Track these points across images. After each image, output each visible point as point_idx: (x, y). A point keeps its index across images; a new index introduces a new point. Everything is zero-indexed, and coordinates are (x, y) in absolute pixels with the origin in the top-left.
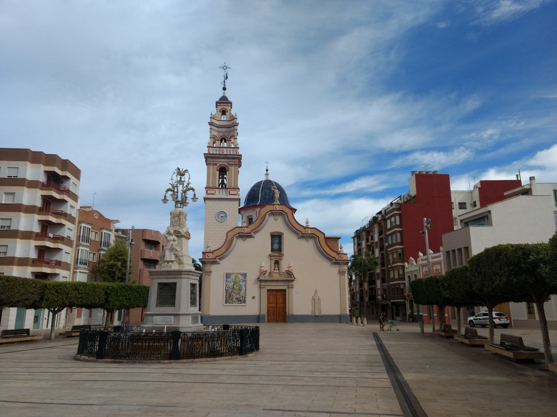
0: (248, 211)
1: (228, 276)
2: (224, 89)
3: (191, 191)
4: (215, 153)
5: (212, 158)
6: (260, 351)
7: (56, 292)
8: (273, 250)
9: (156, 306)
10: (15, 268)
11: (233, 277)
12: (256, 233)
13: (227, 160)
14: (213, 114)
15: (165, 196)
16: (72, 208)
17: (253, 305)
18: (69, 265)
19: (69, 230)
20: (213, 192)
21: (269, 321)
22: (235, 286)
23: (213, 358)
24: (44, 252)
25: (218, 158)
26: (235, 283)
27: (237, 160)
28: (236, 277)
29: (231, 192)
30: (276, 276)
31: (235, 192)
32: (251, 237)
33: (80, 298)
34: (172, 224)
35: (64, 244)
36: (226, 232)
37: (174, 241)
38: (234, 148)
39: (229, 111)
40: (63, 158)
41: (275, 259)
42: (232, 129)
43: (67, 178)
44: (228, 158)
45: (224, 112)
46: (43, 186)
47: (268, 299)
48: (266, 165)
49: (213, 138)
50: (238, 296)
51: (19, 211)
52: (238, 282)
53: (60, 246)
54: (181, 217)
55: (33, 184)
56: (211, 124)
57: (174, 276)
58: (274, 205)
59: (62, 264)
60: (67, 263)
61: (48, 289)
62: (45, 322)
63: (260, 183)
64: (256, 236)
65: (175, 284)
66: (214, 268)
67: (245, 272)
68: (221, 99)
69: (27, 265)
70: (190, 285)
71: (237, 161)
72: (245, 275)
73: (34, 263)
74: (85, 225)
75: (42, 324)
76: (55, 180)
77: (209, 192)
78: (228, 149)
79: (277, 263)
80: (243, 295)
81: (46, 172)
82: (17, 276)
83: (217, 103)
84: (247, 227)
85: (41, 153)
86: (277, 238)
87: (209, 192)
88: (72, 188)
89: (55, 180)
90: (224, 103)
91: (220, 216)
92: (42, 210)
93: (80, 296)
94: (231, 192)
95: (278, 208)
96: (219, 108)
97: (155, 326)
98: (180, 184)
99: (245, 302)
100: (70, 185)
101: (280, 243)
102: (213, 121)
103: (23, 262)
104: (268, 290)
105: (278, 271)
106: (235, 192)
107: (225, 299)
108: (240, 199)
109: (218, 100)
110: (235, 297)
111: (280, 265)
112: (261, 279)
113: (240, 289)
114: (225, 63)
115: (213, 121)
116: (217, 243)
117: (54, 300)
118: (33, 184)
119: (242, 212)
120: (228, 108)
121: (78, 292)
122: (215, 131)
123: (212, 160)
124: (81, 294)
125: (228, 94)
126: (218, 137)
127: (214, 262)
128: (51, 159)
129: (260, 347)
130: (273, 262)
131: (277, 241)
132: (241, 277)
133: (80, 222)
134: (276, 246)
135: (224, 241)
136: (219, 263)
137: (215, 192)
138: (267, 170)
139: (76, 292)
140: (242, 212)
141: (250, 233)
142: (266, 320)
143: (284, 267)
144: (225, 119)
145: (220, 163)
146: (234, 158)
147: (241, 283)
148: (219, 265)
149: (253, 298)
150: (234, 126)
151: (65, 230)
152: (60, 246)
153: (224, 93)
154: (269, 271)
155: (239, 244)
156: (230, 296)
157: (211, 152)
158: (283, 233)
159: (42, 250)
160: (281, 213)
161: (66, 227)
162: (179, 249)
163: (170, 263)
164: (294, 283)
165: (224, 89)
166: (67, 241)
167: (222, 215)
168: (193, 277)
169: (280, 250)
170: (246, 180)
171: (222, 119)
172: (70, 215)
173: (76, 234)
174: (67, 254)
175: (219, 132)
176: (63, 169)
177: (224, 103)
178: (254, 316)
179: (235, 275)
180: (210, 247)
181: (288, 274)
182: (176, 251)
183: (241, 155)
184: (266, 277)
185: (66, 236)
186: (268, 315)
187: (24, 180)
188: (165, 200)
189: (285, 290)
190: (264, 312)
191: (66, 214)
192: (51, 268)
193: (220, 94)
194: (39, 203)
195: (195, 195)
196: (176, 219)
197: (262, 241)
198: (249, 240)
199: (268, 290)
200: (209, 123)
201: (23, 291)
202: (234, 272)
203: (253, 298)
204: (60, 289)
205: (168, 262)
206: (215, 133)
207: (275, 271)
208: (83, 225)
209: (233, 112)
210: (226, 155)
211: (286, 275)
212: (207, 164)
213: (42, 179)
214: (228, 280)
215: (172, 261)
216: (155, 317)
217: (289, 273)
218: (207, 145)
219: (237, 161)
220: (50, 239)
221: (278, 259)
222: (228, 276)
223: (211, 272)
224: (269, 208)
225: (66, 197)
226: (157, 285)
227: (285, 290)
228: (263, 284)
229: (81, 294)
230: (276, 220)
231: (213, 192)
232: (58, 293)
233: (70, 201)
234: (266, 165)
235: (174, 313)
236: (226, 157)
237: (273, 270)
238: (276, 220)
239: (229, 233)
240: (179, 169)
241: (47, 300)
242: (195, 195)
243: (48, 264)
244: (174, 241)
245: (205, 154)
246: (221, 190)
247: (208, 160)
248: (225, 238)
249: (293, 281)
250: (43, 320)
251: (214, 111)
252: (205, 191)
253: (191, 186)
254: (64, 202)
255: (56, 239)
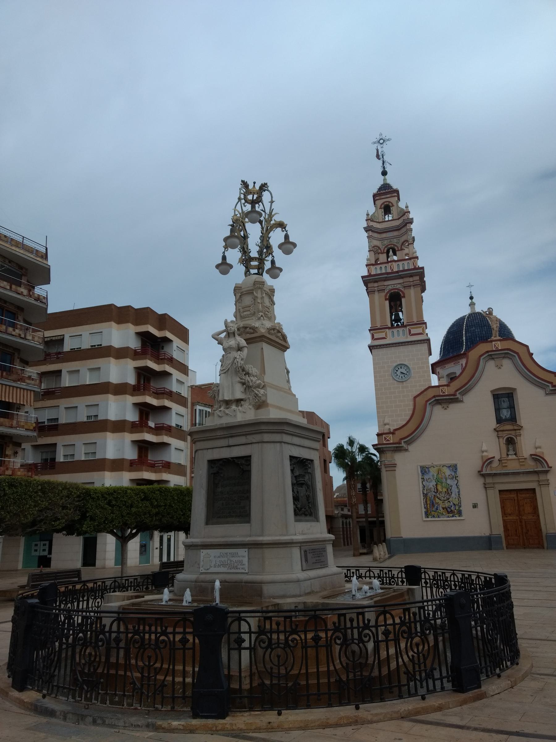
0: (447, 366)
1: (424, 470)
2: (384, 173)
3: (279, 229)
4: (379, 272)
5: (376, 281)
6: (524, 664)
7: (109, 503)
8: (499, 420)
9: (207, 523)
10: (107, 474)
11: (433, 471)
12: (464, 393)
13: (400, 281)
14: (371, 213)
15: (224, 258)
16: (176, 383)
17: (478, 517)
18: (184, 467)
19: (178, 416)
20: (383, 335)
21: (509, 546)
22: (439, 488)
23: (348, 711)
24: (147, 450)
25: (386, 279)
26: (438, 481)
27: (417, 277)
28: (439, 472)
29: (413, 331)
30: (513, 466)
31: (419, 330)
32: (456, 401)
33: (157, 514)
34: (239, 314)
35: (171, 436)
36: (411, 398)
37: (240, 349)
38: (410, 259)
39: (395, 204)
40: (160, 312)
41: (506, 435)
42: (404, 230)
43: (167, 341)
44: (401, 277)
45: (387, 209)
46: (136, 355)
47: (503, 508)
48: (468, 290)
49: (374, 250)
50: (447, 505)
51: (107, 392)
52: (444, 480)
53: (166, 439)
54: (258, 294)
55: (121, 353)
56: (367, 229)
57: (243, 440)
58: (491, 341)
59: (172, 466)
60: (179, 464)
61: (93, 498)
62: (157, 553)
63: (462, 319)
64: (466, 398)
65: (247, 459)
66: (399, 458)
67: (454, 462)
68: (380, 189)
69: (122, 470)
70: (287, 463)
71: (417, 278)
72: (454, 468)
73: (132, 465)
74: (201, 408)
75: (153, 557)
76: (153, 345)
77: (376, 336)
78: (400, 263)
79: (510, 442)
80: (456, 502)
81: (138, 334)
82: (114, 485)
83: (374, 196)
84: (447, 385)
85: (129, 308)
86: (504, 399)
87: (376, 336)
88: (176, 355)
89: (153, 345)
90: (386, 196)
91: (398, 373)
92: (136, 390)
93: (154, 511)
94: (413, 331)
95: (500, 345)
96: (379, 203)
97: (202, 577)
98: (253, 222)
99: (460, 513)
100: (175, 349)
101: (512, 407)
102: (371, 224)
103: (117, 465)
104: (500, 491)
105: (514, 457)
106: (419, 330)
107: (424, 510)
108: (428, 341)
109: (375, 191)
110: (442, 505)
111: (518, 446)
112: (484, 472)
113: (449, 492)
114: (381, 135)
115: (371, 224)
116: (400, 416)
117: (106, 519)
118: (121, 353)
119: (438, 370)
120: (394, 200)
121: (152, 504)
122: (375, 238)
123: (376, 285)
124: (158, 506)
125: (391, 180)
126: (382, 248)
127: (398, 449)
128: (142, 315)
129: (522, 644)
130: (503, 441)
131: (505, 404)
132: (448, 472)
133: (193, 405)
134: (505, 414)
135: (411, 412)
136: (406, 450)
137: (386, 334)
138: (471, 298)
139: (148, 504)
140: (438, 370)
141: (454, 395)
142: (504, 545)
143: (526, 446)
144: (390, 218)
145: (390, 287)
146: (411, 276)
147: (449, 481)
148: (406, 454)
149: (475, 506)
150: (406, 225)
151: (171, 415)
152: (166, 439)
153: (385, 180)
154: (498, 457)
155: (439, 416)
156: (433, 505)
157: (373, 273)
158: (515, 389)
159: (143, 447)
160: (507, 354)
161: (173, 412)
162: (254, 370)
163: (234, 407)
164: (550, 476)
165: (384, 173)
166: (177, 432)
167: (403, 370)
168: (296, 440)
169: (513, 419)
170: (439, 316)
171: (387, 219)
172: (179, 394)
173: (189, 421)
174: (179, 451)
175: (382, 240)
176: (161, 328)
177: (386, 196)
178: (481, 538)
179: (436, 468)
180: (388, 424)
181: (536, 460)
182: (248, 374)
183: (423, 268)
184: (495, 467)
185: (174, 425)
186: (507, 536)
187: (110, 347)
188: (224, 267)
189: (534, 490)
190: (499, 530)
191: (171, 392)
192: (155, 472)
193: (379, 181)
194: (131, 380)
195: (287, 237)
196: (248, 300)
197: (478, 406)
198: (454, 407)
199: (500, 491)
200: (365, 228)
201: (45, 504)
202: (435, 463)
203: (475, 506)
204: (116, 499)
205: (228, 403)
206: (376, 243)
207: (510, 457)
208: (198, 408)
209: (402, 205)
210: (397, 272)
211: (531, 463)
212: (368, 293)
213: (134, 344)
214: (426, 477)
215: (238, 401)
216: (204, 553)
217: (537, 458)
218: (365, 262)
219: (417, 278)
220: (151, 430)
221: (512, 434)
222: (424, 470)
223: (395, 465)
224: (482, 348)
225: (168, 368)
226: (206, 463)
227: (534, 490)
228: (489, 480)
229: (158, 506)
230: (499, 367)
231: (383, 335)
232: (113, 506)
233: (176, 374)
234: (468, 290)
235: (248, 539)
236: (399, 275)
237: (504, 455)
238: (499, 367)
239: (417, 399)
240: (245, 184)
241: (92, 519)
242: (287, 237)
243: (152, 467)
244: (240, 349)
245: (363, 277)
246: (395, 331)
247: (370, 285)
248: (412, 407)
249: (546, 472)
250: (153, 550)
251: (372, 210)
252: (369, 335)
253: (277, 218)
254: (166, 375)
255: (159, 429)
